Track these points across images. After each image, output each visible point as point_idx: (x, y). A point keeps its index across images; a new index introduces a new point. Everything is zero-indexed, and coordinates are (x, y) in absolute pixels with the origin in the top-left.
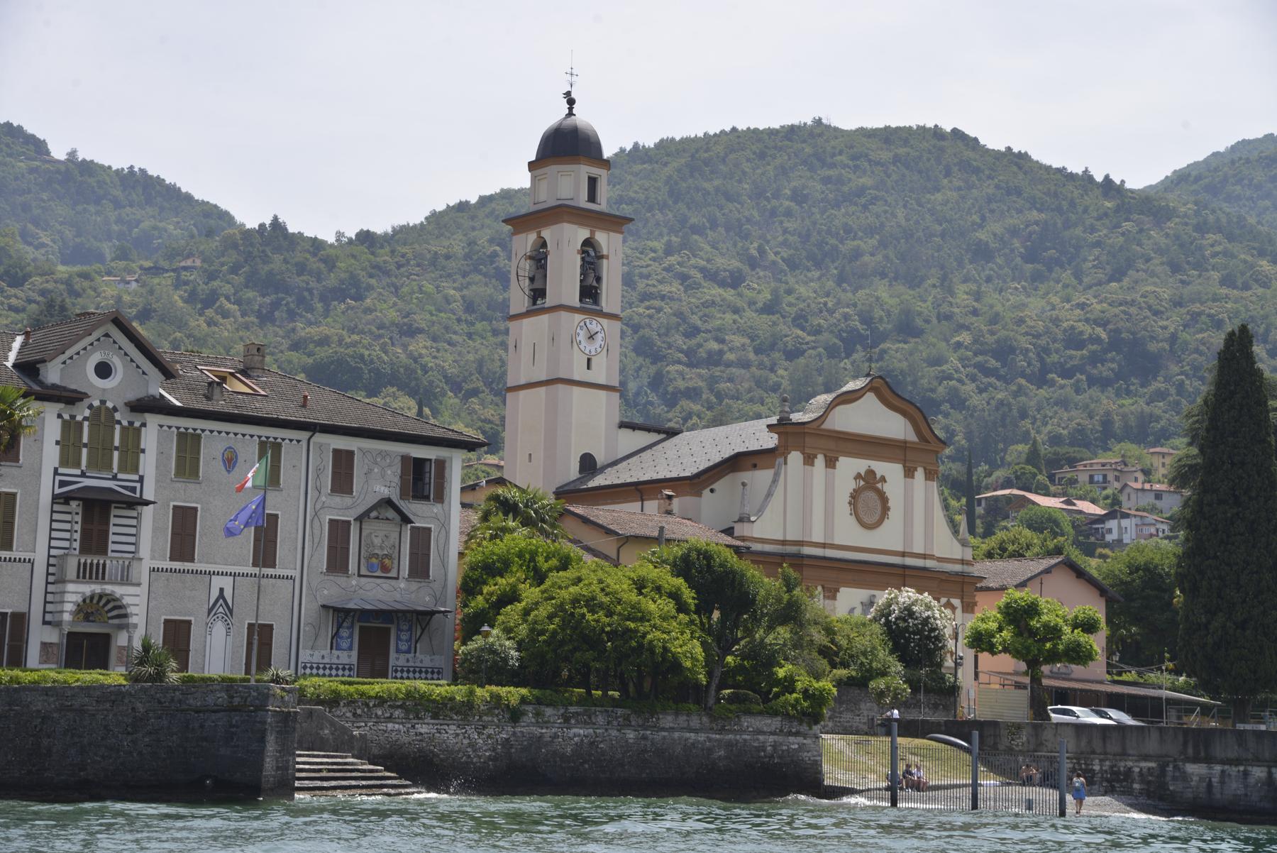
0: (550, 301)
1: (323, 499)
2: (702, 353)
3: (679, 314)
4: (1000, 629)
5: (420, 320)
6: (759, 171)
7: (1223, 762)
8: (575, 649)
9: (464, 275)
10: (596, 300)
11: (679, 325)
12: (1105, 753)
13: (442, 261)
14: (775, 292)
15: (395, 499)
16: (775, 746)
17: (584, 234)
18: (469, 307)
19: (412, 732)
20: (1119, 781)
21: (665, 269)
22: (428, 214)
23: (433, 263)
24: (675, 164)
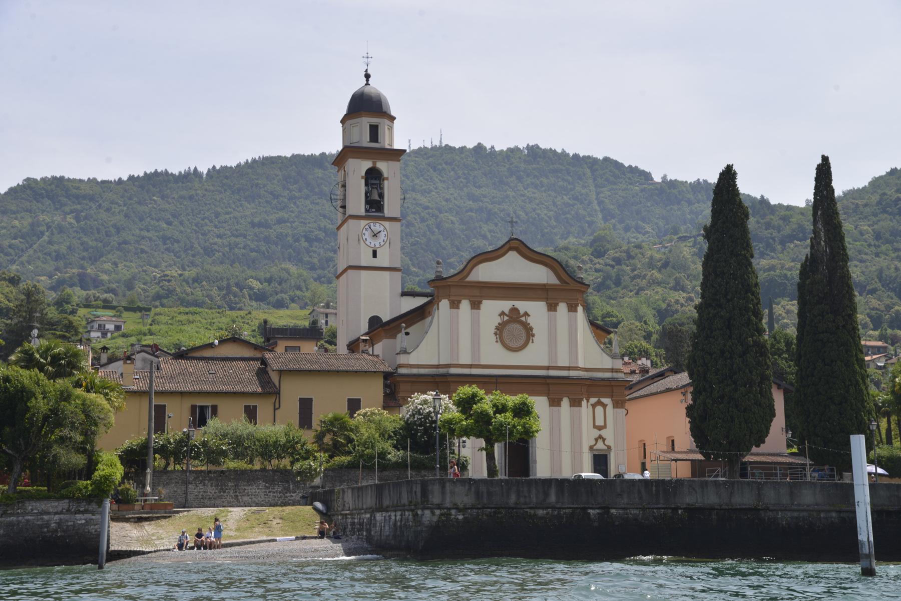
13: (861, 208)
16: (59, 523)
18: (878, 236)
23: (855, 211)
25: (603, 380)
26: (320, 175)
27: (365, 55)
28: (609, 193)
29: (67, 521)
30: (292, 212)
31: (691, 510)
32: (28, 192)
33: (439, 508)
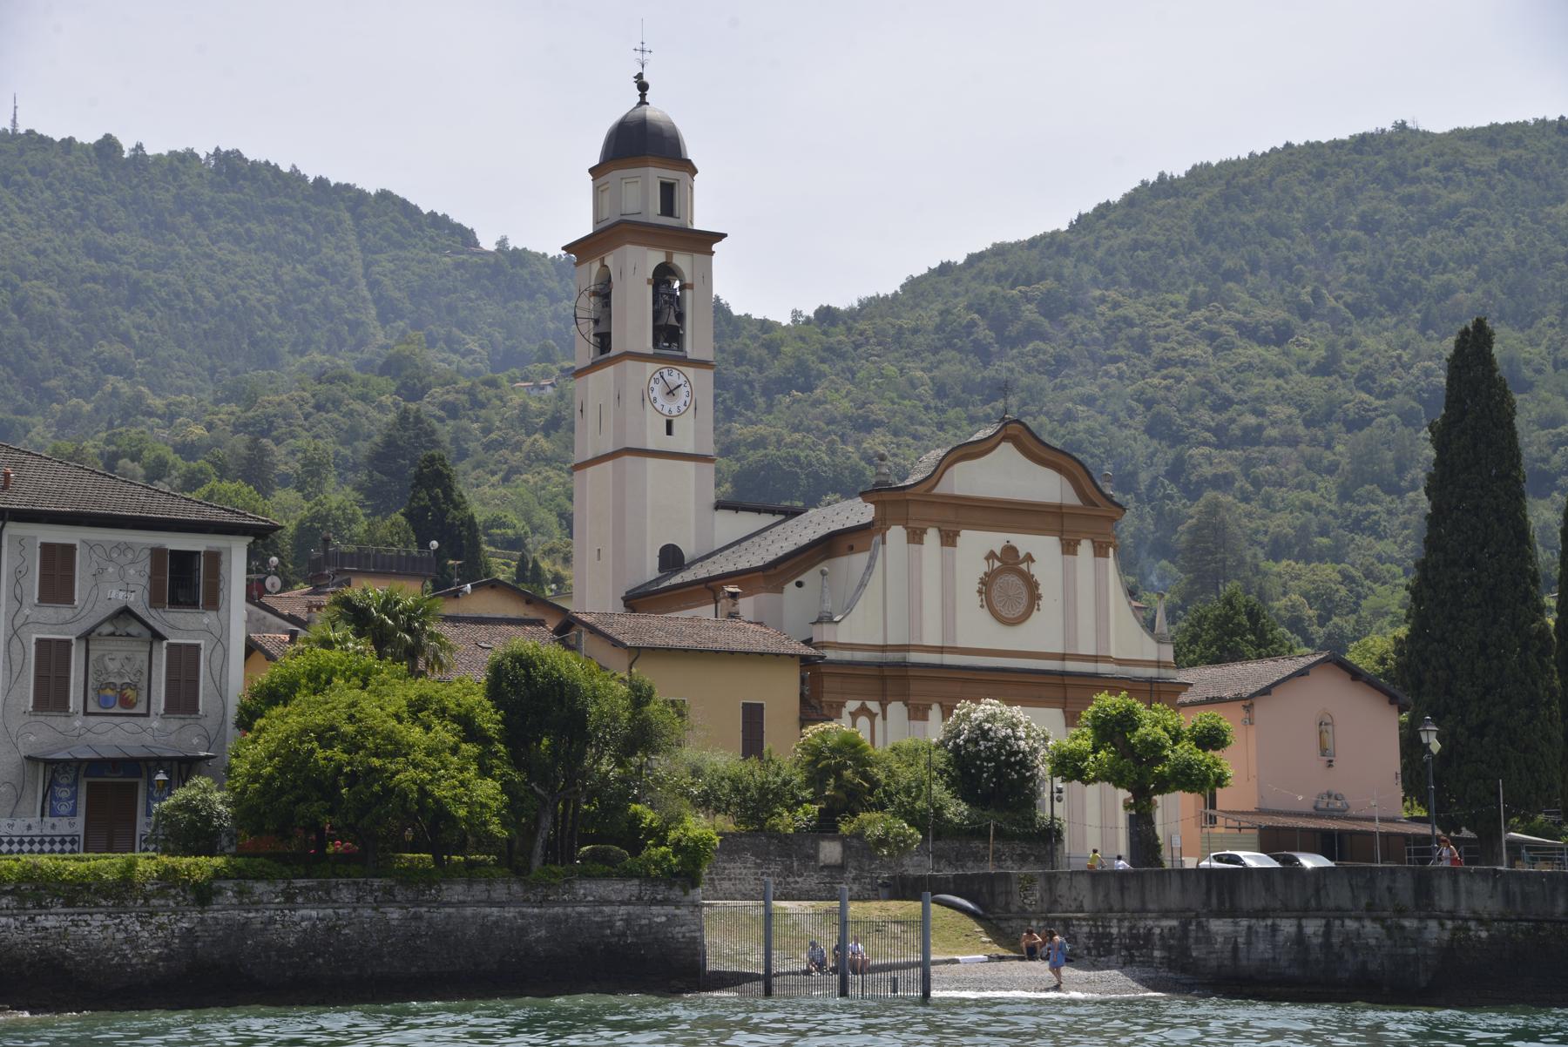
0: (615, 350)
1: (27, 612)
2: (1235, 430)
3: (1205, 383)
4: (1095, 750)
5: (878, 410)
6: (1315, 196)
7: (1249, 915)
8: (299, 800)
9: (935, 351)
11: (1205, 396)
12: (1123, 910)
13: (908, 335)
14: (1331, 347)
15: (140, 610)
16: (628, 920)
17: (656, 257)
18: (941, 391)
19: (30, 927)
20: (1139, 948)
21: (1189, 328)
22: (904, 281)
24: (1207, 196)
27: (639, 46)
28: (392, 266)
29: (639, 917)
33: (1453, 918)
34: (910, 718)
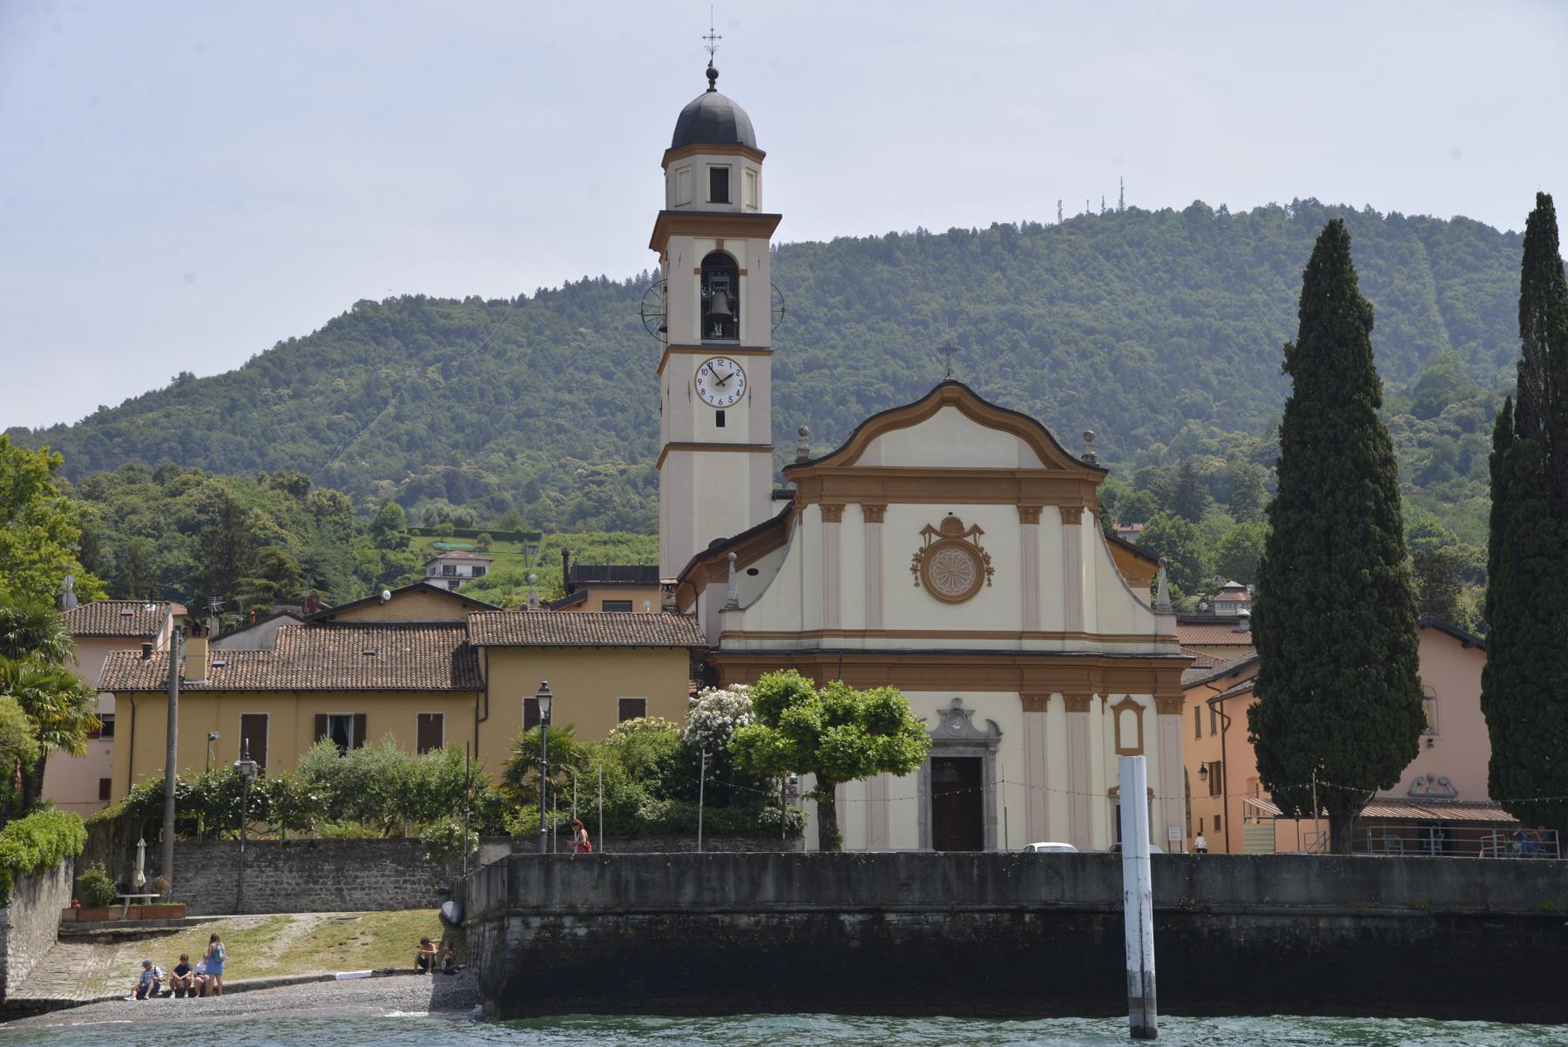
10: (731, 328)
25: (1134, 657)
26: (886, 276)
27: (708, 34)
28: (1465, 289)
30: (833, 347)
31: (1050, 914)
32: (362, 326)
34: (1025, 710)
